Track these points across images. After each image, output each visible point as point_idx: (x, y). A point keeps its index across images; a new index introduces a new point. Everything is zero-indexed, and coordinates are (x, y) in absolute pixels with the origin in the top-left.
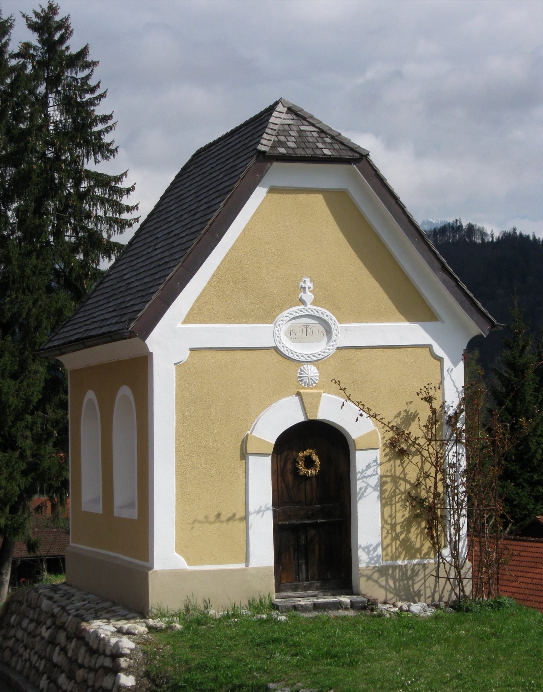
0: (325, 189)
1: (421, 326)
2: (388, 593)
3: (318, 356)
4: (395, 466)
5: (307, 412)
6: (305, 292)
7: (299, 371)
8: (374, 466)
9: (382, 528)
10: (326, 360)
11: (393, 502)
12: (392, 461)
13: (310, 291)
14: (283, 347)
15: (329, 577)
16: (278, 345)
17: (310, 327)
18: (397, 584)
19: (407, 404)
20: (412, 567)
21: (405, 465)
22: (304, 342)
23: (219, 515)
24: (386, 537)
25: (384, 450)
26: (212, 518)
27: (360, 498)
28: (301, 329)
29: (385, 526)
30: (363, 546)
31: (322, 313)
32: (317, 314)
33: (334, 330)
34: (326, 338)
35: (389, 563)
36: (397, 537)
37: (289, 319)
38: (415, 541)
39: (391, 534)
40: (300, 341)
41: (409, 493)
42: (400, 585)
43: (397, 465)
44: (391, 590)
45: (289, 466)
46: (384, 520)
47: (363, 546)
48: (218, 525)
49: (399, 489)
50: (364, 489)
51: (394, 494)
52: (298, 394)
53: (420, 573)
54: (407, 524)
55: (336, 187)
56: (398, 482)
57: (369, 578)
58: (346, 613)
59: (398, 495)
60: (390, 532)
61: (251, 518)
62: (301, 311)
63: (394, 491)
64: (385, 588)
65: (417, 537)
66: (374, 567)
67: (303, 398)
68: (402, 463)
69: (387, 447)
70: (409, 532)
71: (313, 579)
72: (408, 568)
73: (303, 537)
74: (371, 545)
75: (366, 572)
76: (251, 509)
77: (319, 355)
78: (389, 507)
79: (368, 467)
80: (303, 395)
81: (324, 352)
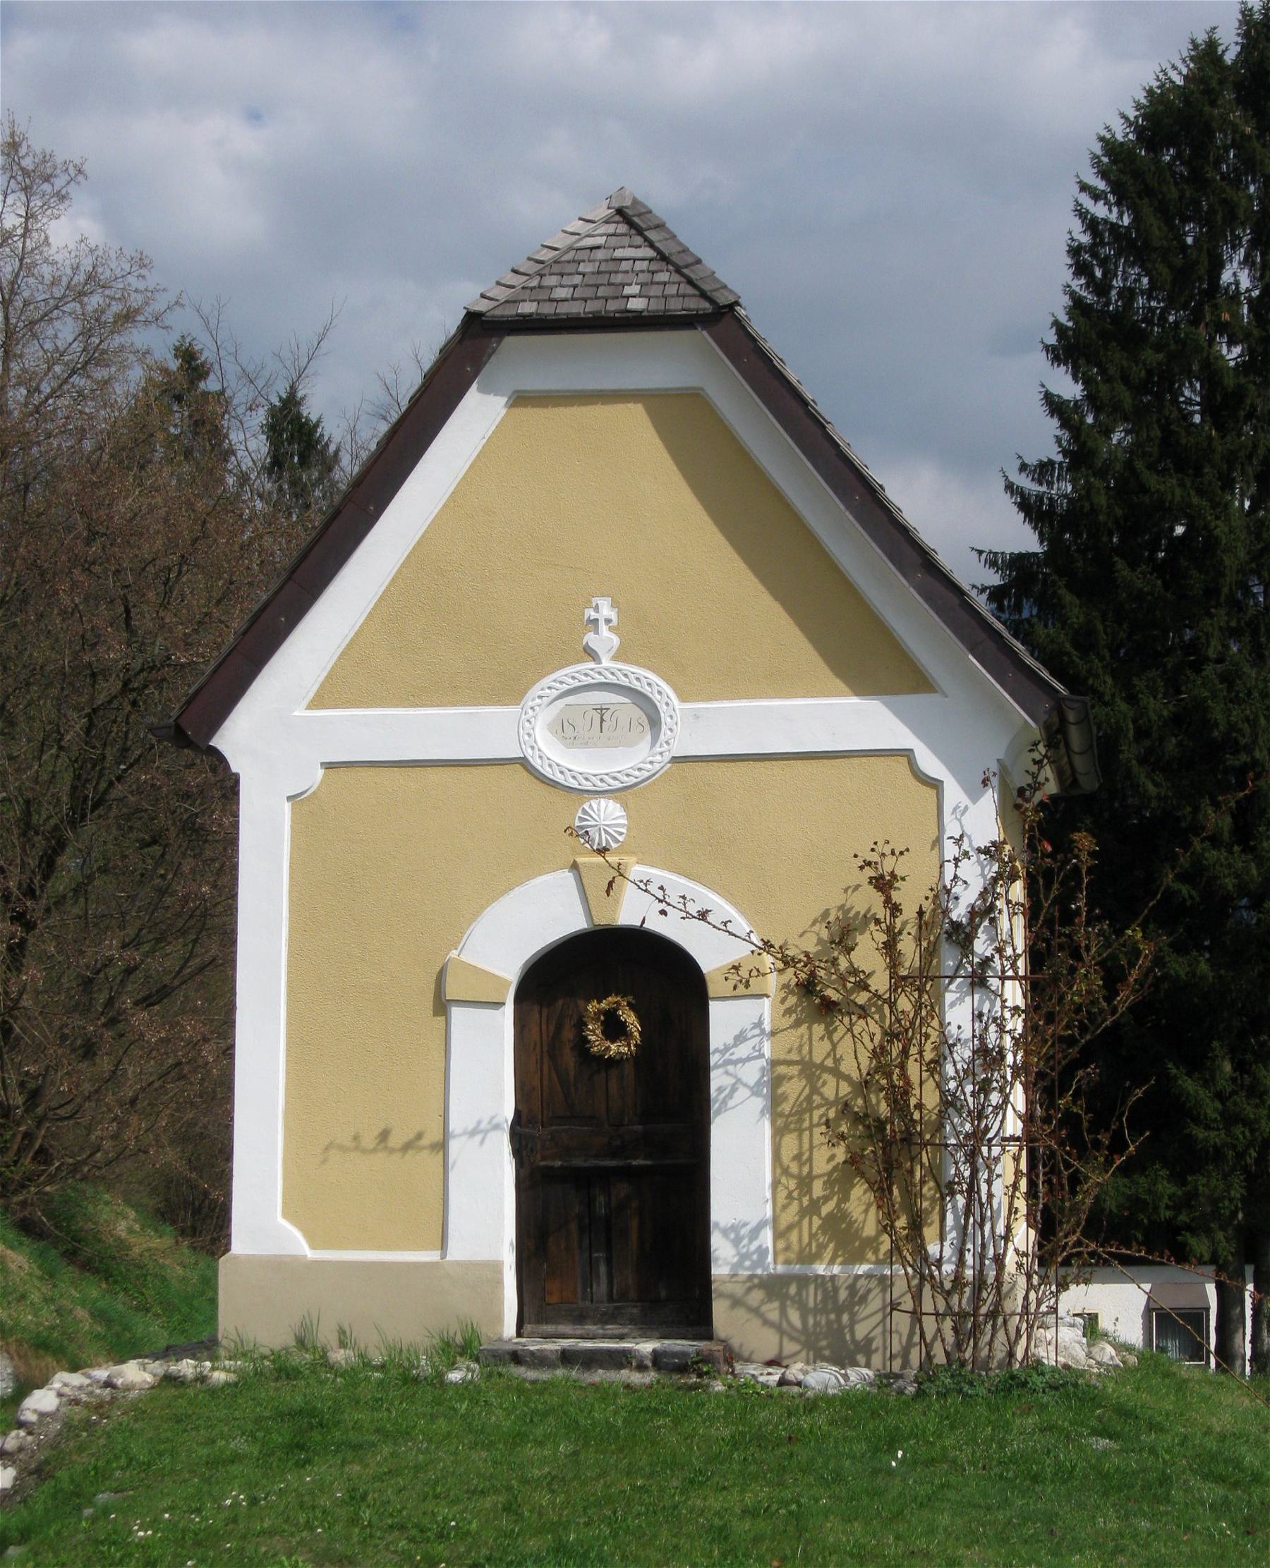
0: (649, 390)
1: (886, 704)
2: (785, 1340)
3: (626, 779)
4: (810, 1039)
5: (592, 908)
6: (597, 632)
7: (580, 814)
8: (754, 1036)
9: (775, 1184)
10: (645, 788)
11: (806, 1124)
12: (805, 1026)
13: (610, 629)
14: (541, 757)
15: (663, 1294)
16: (528, 752)
17: (609, 712)
18: (811, 1321)
19: (846, 891)
20: (850, 1281)
21: (836, 1037)
22: (595, 746)
23: (384, 1135)
24: (785, 1207)
25: (783, 1001)
26: (369, 1140)
27: (719, 1112)
28: (588, 717)
29: (784, 1180)
30: (722, 1224)
31: (638, 679)
32: (624, 681)
33: (665, 718)
34: (649, 737)
35: (797, 1269)
36: (814, 1207)
37: (555, 693)
38: (861, 1218)
39: (800, 1200)
40: (586, 745)
41: (846, 1105)
42: (816, 1324)
43: (815, 1038)
44: (795, 1334)
45: (568, 1034)
46: (781, 1165)
47: (722, 1224)
48: (381, 1155)
49: (821, 1094)
50: (727, 1091)
51: (806, 1106)
52: (575, 867)
53: (871, 1297)
54: (841, 1180)
55: (670, 386)
56: (819, 1078)
57: (736, 1302)
58: (636, 1378)
59: (818, 1107)
60: (795, 1194)
61: (454, 1146)
62: (586, 675)
63: (809, 1099)
64: (778, 1328)
65: (866, 1211)
66: (751, 1277)
67: (583, 875)
68: (830, 1034)
69: (791, 992)
70: (845, 1198)
71: (623, 1296)
72: (839, 1283)
73: (601, 1199)
74: (745, 1224)
75: (729, 1288)
76: (455, 1125)
77: (628, 775)
78: (794, 1135)
79: (740, 1038)
80: (582, 869)
81: (640, 769)
